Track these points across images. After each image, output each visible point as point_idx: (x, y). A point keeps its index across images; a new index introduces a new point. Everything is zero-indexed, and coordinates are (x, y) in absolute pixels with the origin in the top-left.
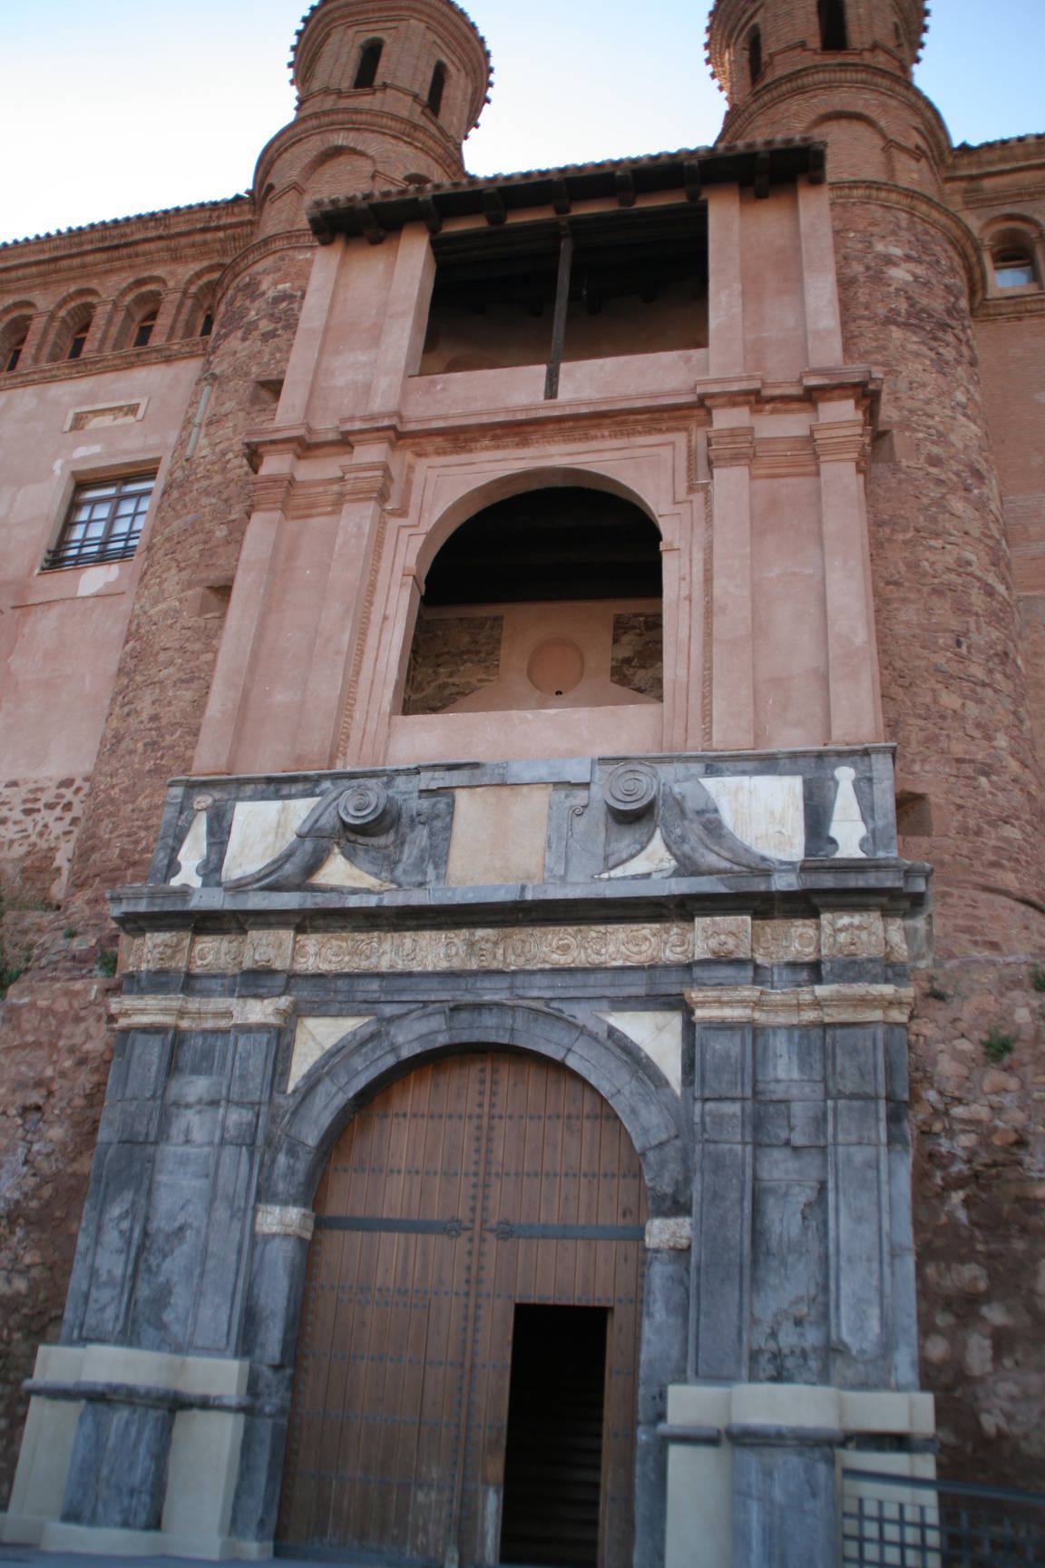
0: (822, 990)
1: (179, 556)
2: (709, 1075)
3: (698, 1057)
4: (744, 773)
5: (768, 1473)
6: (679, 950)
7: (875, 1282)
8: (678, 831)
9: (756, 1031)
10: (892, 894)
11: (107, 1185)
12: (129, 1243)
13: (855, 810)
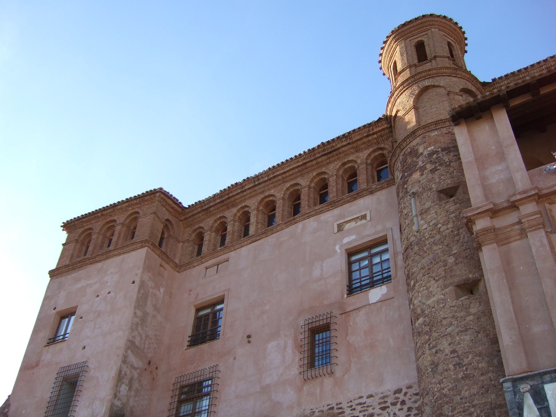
1: (434, 275)
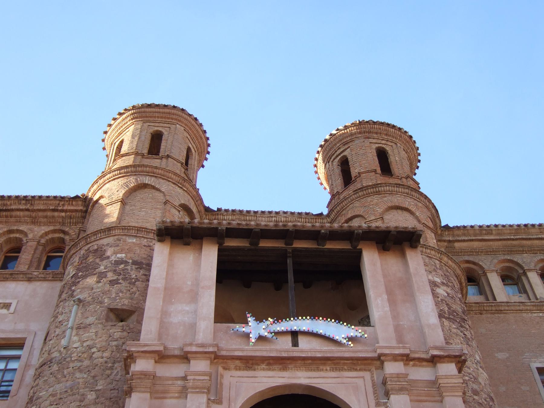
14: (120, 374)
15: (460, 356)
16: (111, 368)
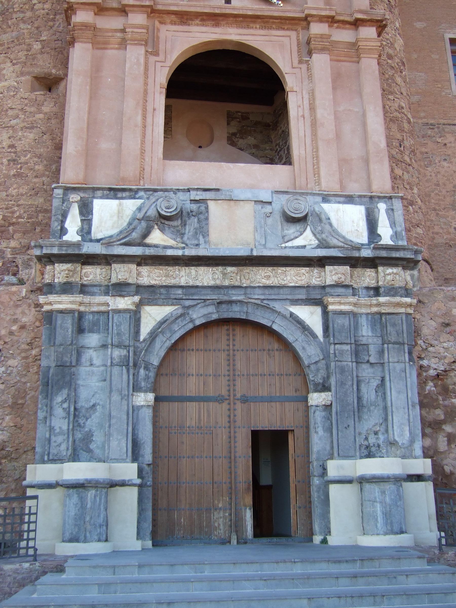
0: (382, 299)
2: (336, 334)
3: (331, 325)
4: (339, 202)
5: (383, 492)
6: (318, 279)
7: (406, 417)
8: (320, 228)
9: (355, 315)
10: (408, 260)
11: (52, 387)
12: (69, 413)
13: (387, 223)
14: (62, 26)
15: (381, 21)
16: (53, 20)
